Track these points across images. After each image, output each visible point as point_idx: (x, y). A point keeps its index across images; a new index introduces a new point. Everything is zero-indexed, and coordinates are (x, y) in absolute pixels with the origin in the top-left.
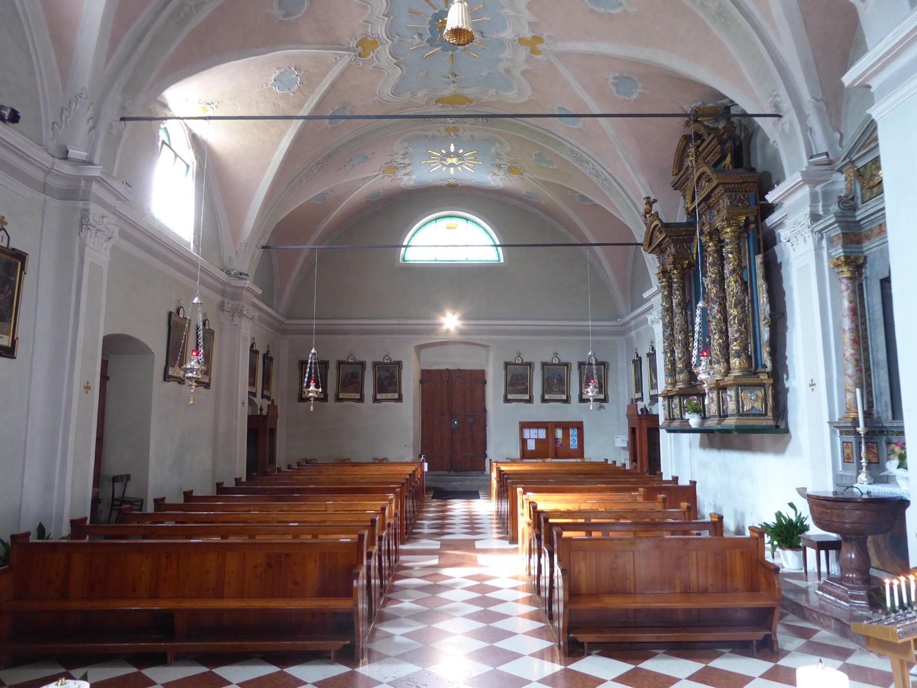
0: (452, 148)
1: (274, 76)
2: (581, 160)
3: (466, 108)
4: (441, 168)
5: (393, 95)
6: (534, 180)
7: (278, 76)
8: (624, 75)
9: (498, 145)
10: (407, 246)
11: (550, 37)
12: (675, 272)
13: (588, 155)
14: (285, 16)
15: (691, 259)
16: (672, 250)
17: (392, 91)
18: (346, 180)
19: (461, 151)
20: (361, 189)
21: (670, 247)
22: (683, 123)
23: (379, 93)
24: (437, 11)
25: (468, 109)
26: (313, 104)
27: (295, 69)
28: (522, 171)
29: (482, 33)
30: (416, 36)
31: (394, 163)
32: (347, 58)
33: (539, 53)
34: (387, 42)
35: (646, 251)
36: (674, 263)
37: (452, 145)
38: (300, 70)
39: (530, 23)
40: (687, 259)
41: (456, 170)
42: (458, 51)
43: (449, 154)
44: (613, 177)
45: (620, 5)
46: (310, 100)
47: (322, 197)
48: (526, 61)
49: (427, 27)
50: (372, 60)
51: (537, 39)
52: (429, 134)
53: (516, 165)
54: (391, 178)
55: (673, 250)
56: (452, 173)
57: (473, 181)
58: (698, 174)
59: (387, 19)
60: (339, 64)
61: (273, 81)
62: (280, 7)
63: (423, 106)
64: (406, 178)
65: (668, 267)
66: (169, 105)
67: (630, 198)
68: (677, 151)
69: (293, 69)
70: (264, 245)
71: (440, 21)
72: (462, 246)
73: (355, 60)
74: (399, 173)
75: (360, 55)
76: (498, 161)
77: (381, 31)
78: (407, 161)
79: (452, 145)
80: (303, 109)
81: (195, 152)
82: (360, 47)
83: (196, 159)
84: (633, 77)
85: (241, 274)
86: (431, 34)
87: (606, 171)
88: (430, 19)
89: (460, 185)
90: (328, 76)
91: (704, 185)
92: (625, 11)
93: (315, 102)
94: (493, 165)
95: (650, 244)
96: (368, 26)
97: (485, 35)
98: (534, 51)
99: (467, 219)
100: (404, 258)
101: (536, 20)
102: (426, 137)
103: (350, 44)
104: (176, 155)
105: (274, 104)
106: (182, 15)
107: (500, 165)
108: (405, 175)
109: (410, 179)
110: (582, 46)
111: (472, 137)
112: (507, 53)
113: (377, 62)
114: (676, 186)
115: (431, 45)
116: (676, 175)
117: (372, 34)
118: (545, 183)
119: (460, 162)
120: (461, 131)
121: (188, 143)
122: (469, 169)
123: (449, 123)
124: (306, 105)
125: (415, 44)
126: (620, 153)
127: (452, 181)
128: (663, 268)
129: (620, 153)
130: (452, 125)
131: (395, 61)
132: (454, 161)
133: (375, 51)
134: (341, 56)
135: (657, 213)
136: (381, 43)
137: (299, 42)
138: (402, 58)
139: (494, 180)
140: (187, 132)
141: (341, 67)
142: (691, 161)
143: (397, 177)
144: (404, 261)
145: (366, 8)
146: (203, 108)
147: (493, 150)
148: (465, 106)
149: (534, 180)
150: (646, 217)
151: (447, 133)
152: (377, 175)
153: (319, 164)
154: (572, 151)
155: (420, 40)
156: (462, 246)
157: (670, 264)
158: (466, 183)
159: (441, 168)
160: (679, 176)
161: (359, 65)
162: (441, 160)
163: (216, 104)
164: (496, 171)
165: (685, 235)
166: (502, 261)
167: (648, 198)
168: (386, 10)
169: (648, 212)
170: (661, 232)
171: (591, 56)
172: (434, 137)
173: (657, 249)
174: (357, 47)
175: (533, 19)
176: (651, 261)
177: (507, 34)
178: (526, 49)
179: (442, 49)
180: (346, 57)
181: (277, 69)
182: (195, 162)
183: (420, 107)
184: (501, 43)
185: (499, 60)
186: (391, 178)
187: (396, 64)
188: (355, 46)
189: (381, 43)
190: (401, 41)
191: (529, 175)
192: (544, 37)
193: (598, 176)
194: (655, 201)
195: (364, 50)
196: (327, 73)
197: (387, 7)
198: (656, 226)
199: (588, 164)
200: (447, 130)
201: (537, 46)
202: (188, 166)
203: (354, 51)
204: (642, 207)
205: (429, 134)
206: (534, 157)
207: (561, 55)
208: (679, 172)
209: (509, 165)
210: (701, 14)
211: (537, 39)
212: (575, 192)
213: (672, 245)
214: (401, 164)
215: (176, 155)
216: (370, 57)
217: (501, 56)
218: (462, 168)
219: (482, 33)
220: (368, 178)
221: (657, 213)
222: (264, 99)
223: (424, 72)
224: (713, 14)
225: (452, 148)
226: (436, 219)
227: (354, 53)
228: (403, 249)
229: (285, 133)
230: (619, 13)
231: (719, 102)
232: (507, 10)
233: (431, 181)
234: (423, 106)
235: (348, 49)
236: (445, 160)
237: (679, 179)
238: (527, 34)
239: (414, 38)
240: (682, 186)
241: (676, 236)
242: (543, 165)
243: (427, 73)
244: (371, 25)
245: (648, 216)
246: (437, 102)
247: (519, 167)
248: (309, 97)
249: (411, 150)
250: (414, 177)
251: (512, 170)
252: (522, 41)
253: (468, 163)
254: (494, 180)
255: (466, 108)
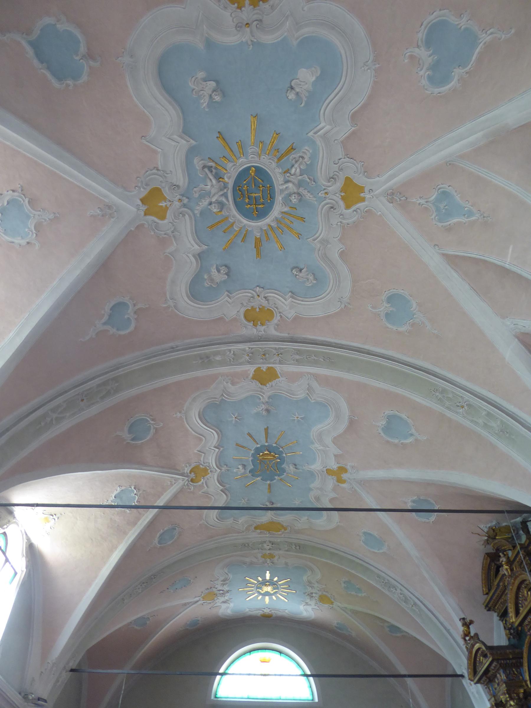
0: (268, 576)
1: (115, 493)
2: (389, 585)
3: (281, 535)
4: (257, 597)
5: (218, 520)
6: (344, 609)
7: (119, 493)
8: (421, 498)
9: (309, 573)
10: (222, 674)
11: (353, 467)
12: (512, 703)
13: (395, 580)
14: (133, 439)
15: (526, 688)
16: (502, 676)
17: (218, 516)
18: (168, 605)
19: (276, 579)
20: (182, 614)
21: (499, 674)
22: (482, 543)
23: (205, 517)
24: (259, 446)
25: (283, 536)
26: (146, 522)
27: (135, 488)
28: (332, 600)
29: (295, 465)
30: (240, 467)
31: (214, 589)
32: (181, 482)
33: (344, 482)
34: (216, 470)
35: (472, 680)
36: (509, 692)
37: (268, 572)
38: (139, 490)
39: (335, 456)
40: (522, 686)
41: (271, 599)
42: (275, 481)
43: (264, 583)
44: (421, 602)
45: (412, 435)
46: (144, 518)
47: (142, 621)
48: (334, 490)
49: (250, 459)
50: (202, 486)
51: (343, 469)
52: (247, 560)
53: (327, 594)
54: (210, 606)
55: (504, 677)
56: (267, 603)
57: (286, 611)
58: (517, 582)
59: (217, 450)
60: (174, 486)
61: (113, 498)
62: (130, 432)
63: (243, 532)
64: (224, 606)
65: (503, 698)
66: (15, 512)
67: (442, 624)
68: (482, 569)
69: (133, 487)
70: (74, 668)
71: (261, 454)
72: (275, 675)
73: (187, 484)
74: (218, 600)
75: (192, 481)
76: (310, 590)
77: (212, 461)
78: (226, 588)
79: (268, 572)
80: (136, 526)
81: (28, 562)
82: (193, 473)
83: (26, 568)
84: (429, 499)
85: (39, 699)
86: (253, 465)
87: (414, 595)
88: (253, 452)
89: (274, 615)
90: (162, 497)
91: (526, 595)
92: (416, 440)
93: (148, 520)
94: (305, 593)
95: (475, 672)
96: (201, 455)
97: (298, 467)
98: (340, 481)
99: (280, 652)
100: (216, 694)
101: (341, 453)
102: (245, 563)
103: (184, 470)
104: (7, 560)
105: (111, 519)
106: (43, 424)
107: (312, 593)
108: (224, 602)
109: (228, 608)
110: (381, 474)
111: (286, 564)
112: (316, 484)
113: (206, 488)
114: (489, 607)
115: (252, 475)
116: (487, 594)
117: (204, 463)
118: (355, 613)
119: (274, 591)
120: (277, 557)
121: (23, 551)
122: (283, 598)
123: (265, 549)
124: (139, 523)
125: (239, 474)
126: (426, 575)
127: (267, 611)
128: (495, 700)
129: (426, 575)
130: (268, 552)
131: (221, 487)
132: (269, 589)
133: (206, 477)
134: (176, 480)
135: (476, 635)
136: (211, 472)
137: (141, 464)
138: (227, 486)
139: (306, 610)
140: (25, 541)
141: (175, 490)
142: (507, 570)
143: (215, 605)
144: (216, 697)
145: (201, 440)
146: (46, 519)
147: (305, 578)
148: (280, 533)
149: (344, 609)
150: (465, 640)
151: (263, 559)
152: (197, 601)
153: (144, 583)
154: (379, 576)
155: (243, 470)
156: (275, 675)
157: (504, 694)
158: (280, 614)
159: (257, 597)
160: (491, 594)
161: (190, 489)
162: (257, 588)
163: (57, 516)
164: (308, 601)
165: (513, 658)
166: (316, 700)
167: (464, 619)
168: (217, 443)
169: (466, 634)
170: (485, 656)
171: (389, 481)
172: (252, 564)
173: (484, 678)
174: (190, 473)
175: (338, 452)
176: (477, 695)
177: (317, 466)
178: (333, 479)
179: (261, 479)
180: (180, 481)
181: (119, 486)
182: (25, 570)
183: (241, 533)
184: (312, 474)
185: (311, 489)
186: (210, 606)
187: (222, 491)
188: (188, 472)
189: (211, 472)
190: (228, 470)
191: (339, 604)
192: (348, 467)
193: (406, 601)
194: (471, 622)
195: (196, 476)
196: (162, 494)
197: (218, 440)
198: (479, 649)
199: (396, 590)
200: (264, 556)
201: (342, 475)
202: (16, 574)
203: (187, 476)
204: (461, 629)
205: (247, 560)
206: (343, 585)
207: (363, 483)
208: (489, 590)
209: (320, 593)
210: (484, 433)
211: (343, 469)
212: (385, 621)
213: (501, 671)
214: (220, 590)
215: (7, 560)
216: (200, 483)
217: (312, 486)
218: (277, 597)
219: (295, 465)
220: (188, 603)
221: (476, 635)
222: (103, 514)
223: (246, 500)
224: (497, 432)
225: (268, 576)
226: (250, 651)
227: (187, 478)
228: (218, 677)
229: (116, 548)
230: (411, 442)
231: (512, 521)
232: (317, 445)
233: (248, 610)
234: (243, 532)
235: (182, 474)
236: (261, 588)
237: (491, 598)
238: (333, 465)
239: (239, 468)
240: (495, 605)
241: (503, 659)
242: (353, 593)
243: (248, 500)
244: (203, 454)
245: (467, 638)
246: (256, 528)
247: (329, 596)
248: (144, 515)
249: (231, 576)
250: (232, 605)
251: (323, 599)
252: (329, 472)
253: (282, 592)
254: (306, 610)
255: (281, 535)
